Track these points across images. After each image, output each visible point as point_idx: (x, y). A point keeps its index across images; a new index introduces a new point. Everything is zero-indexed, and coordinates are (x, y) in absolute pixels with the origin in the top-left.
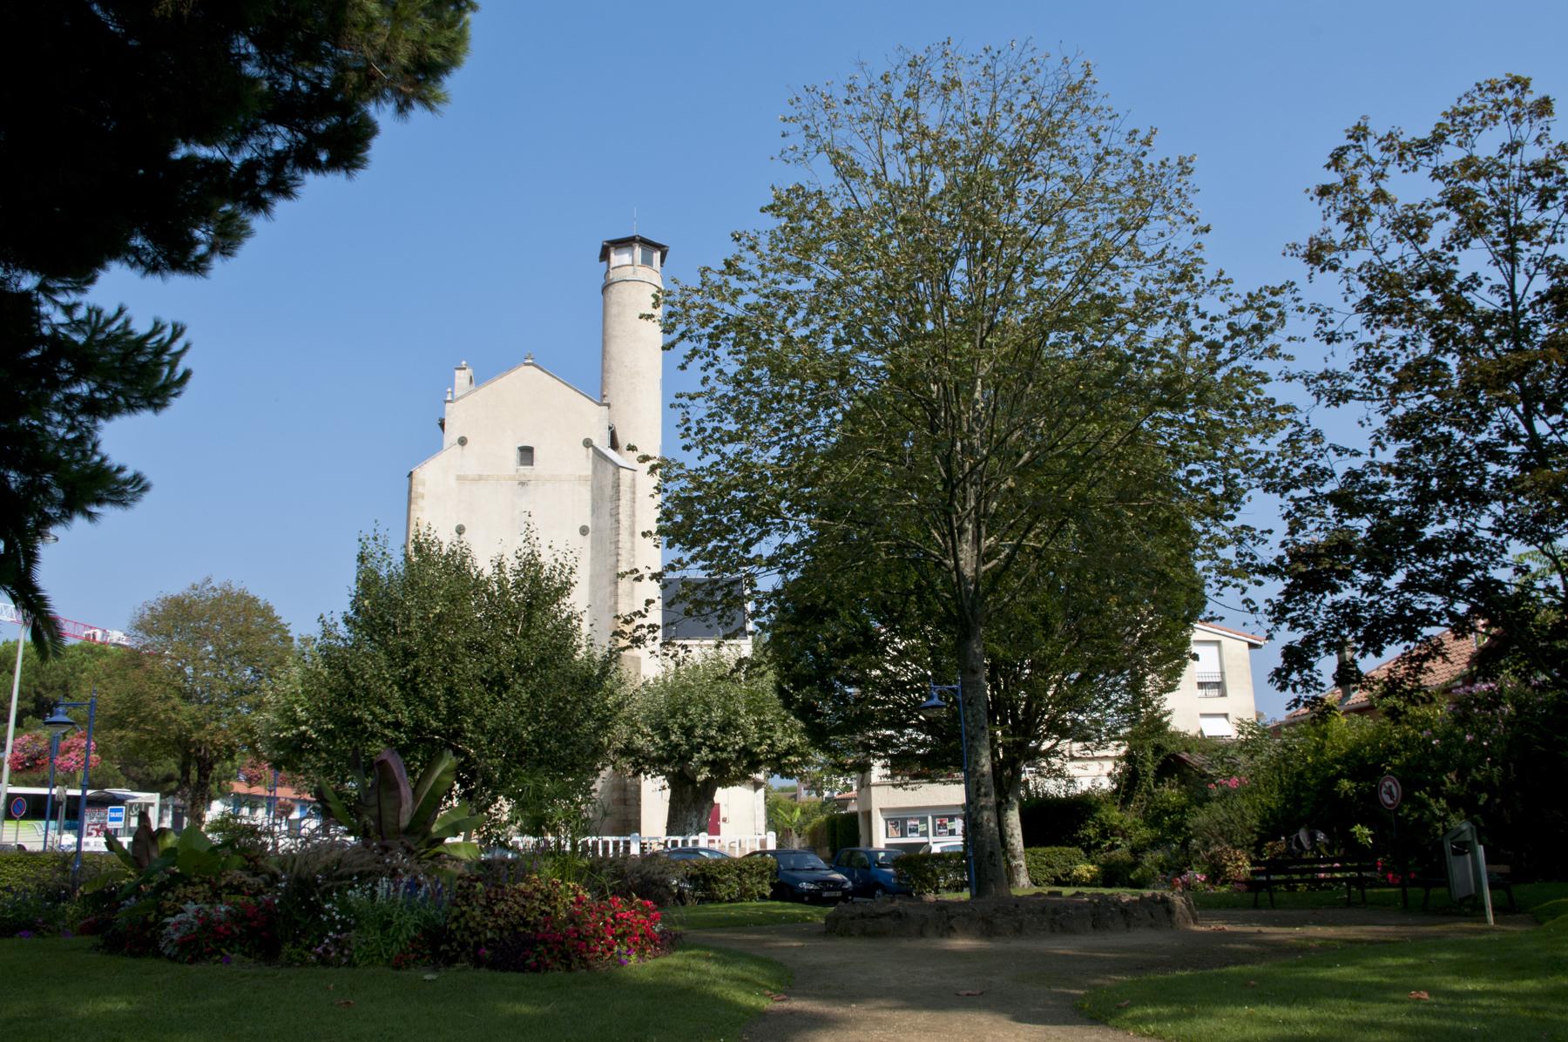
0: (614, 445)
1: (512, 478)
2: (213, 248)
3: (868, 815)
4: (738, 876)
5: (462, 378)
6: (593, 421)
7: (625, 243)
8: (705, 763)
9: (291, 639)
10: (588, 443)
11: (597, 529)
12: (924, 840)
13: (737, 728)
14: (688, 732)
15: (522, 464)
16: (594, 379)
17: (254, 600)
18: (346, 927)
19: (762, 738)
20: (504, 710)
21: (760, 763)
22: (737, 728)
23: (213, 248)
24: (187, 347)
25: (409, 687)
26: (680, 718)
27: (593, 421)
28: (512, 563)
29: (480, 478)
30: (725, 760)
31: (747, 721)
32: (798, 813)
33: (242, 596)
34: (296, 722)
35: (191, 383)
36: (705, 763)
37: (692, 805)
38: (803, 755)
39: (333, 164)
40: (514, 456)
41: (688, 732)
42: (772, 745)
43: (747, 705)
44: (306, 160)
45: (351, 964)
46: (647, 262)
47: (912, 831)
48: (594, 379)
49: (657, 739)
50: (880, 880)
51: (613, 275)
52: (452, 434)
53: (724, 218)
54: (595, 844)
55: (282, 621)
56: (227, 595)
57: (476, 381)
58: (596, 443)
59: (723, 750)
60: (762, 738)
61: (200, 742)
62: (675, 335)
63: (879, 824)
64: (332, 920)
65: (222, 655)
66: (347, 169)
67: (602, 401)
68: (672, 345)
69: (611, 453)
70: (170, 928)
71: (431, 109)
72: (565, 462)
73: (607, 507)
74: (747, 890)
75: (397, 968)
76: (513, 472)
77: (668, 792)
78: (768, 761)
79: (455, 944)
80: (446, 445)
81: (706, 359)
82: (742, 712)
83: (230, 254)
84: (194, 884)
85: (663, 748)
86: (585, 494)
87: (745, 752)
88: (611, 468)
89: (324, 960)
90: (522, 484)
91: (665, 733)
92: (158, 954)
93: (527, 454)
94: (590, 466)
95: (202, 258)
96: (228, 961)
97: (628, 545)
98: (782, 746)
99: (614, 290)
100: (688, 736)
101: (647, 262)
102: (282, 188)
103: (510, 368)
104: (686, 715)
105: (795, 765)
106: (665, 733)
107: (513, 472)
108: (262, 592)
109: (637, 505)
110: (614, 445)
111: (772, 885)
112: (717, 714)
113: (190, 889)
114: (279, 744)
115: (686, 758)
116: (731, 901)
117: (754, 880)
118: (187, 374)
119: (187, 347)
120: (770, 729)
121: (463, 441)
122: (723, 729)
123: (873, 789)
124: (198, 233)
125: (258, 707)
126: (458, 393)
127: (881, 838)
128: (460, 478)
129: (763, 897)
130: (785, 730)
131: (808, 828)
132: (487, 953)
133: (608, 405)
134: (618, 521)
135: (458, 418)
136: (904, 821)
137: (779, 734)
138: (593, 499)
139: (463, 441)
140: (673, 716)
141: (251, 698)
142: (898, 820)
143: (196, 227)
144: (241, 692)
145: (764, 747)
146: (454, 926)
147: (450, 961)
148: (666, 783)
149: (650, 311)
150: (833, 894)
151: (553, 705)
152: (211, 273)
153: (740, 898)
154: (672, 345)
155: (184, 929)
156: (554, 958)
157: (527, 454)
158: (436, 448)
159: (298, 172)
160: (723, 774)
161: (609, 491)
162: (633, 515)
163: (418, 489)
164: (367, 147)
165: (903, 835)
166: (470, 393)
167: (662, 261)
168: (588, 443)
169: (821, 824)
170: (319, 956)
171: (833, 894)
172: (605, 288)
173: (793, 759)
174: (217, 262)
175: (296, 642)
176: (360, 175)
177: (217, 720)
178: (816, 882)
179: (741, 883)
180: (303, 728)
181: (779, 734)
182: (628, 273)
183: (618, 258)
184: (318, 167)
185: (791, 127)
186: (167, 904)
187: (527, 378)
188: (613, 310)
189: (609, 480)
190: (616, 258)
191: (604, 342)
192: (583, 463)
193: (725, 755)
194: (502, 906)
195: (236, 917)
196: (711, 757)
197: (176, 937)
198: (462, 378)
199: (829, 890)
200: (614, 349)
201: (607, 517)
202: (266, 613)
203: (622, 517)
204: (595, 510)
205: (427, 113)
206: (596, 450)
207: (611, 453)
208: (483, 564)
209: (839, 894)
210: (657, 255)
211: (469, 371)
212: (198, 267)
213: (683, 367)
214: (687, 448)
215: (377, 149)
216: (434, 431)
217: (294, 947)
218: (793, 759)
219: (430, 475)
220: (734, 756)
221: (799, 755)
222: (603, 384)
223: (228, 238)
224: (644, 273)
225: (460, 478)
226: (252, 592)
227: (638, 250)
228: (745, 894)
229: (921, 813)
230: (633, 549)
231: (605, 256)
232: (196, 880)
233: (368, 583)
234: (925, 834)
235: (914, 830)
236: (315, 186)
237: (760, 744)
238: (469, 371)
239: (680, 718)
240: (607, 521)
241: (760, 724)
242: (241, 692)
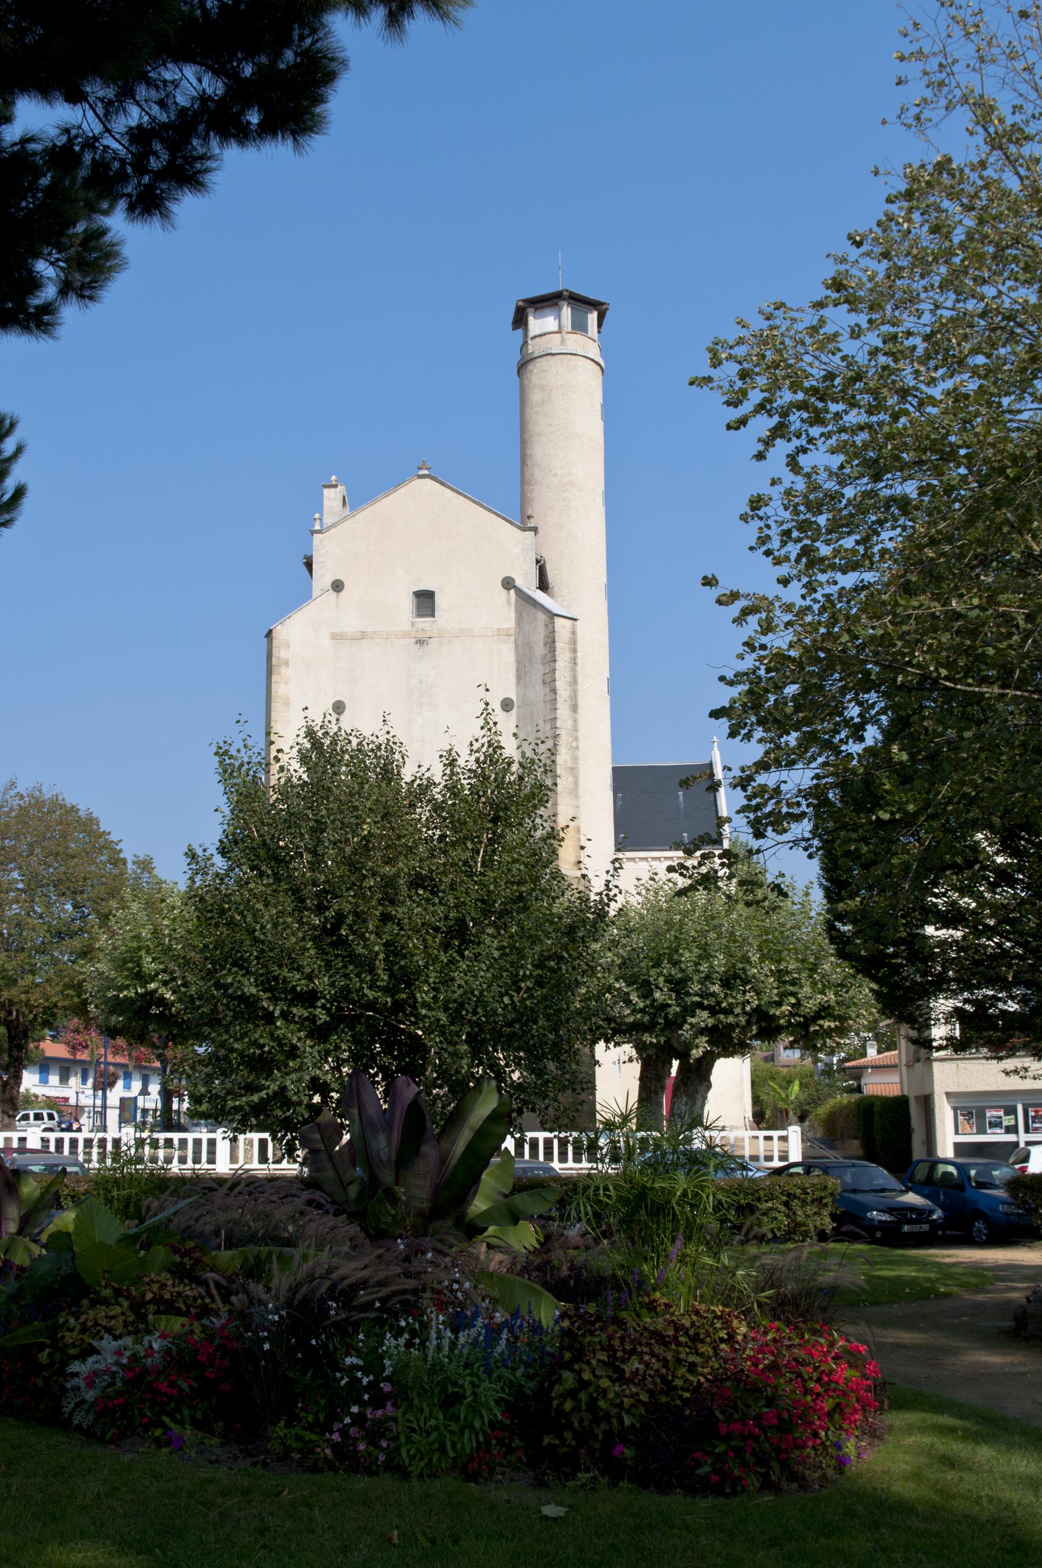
0: (543, 585)
1: (407, 635)
2: (66, 289)
3: (927, 1102)
4: (786, 1204)
5: (332, 498)
6: (512, 552)
7: (547, 302)
8: (702, 1031)
9: (124, 861)
10: (508, 584)
11: (525, 703)
12: (1011, 1138)
13: (746, 982)
14: (678, 986)
15: (420, 614)
16: (511, 492)
17: (74, 809)
18: (379, 1400)
19: (783, 995)
20: (474, 975)
21: (779, 1030)
22: (746, 982)
23: (66, 289)
24: (19, 450)
25: (330, 938)
26: (666, 968)
27: (512, 552)
28: (466, 760)
29: (363, 636)
30: (731, 1027)
31: (760, 970)
32: (796, 1087)
33: (56, 804)
34: (141, 977)
35: (27, 503)
36: (702, 1031)
37: (675, 1083)
38: (842, 1019)
39: (269, 129)
40: (408, 604)
41: (678, 986)
42: (798, 1004)
43: (760, 949)
44: (223, 120)
45: (396, 1468)
46: (580, 326)
47: (993, 1125)
48: (511, 492)
49: (634, 997)
50: (982, 1206)
51: (533, 347)
52: (322, 577)
53: (793, 225)
54: (577, 1159)
55: (113, 838)
56: (38, 803)
57: (353, 503)
58: (519, 583)
59: (728, 1012)
60: (783, 995)
61: (11, 1003)
62: (747, 407)
63: (945, 1116)
64: (355, 1382)
65: (34, 884)
66: (294, 133)
67: (524, 522)
68: (743, 422)
69: (540, 596)
70: (79, 1381)
71: (444, 16)
72: (473, 609)
73: (538, 671)
74: (798, 1225)
75: (472, 1477)
76: (407, 627)
77: (636, 1068)
78: (789, 1027)
79: (568, 1435)
80: (316, 592)
81: (796, 443)
82: (755, 958)
83: (91, 298)
84: (105, 1302)
85: (642, 1011)
86: (507, 656)
87: (760, 1015)
88: (542, 617)
89: (347, 1459)
90: (421, 642)
91: (646, 989)
92: (65, 1425)
93: (425, 601)
94: (512, 615)
95: (47, 309)
96: (178, 1445)
97: (569, 724)
98: (810, 1006)
99: (534, 368)
100: (678, 993)
101: (580, 326)
102: (188, 175)
103: (398, 482)
104: (675, 964)
105: (829, 1033)
106: (646, 989)
107: (407, 627)
108: (82, 797)
109: (579, 667)
110: (543, 585)
111: (833, 1217)
112: (719, 963)
113: (101, 1312)
114: (117, 1006)
115: (674, 1024)
116: (775, 1239)
117: (810, 1210)
118: (19, 493)
119: (19, 450)
120: (793, 983)
121: (338, 586)
122: (727, 983)
123: (936, 1066)
124: (42, 267)
125: (86, 953)
126: (328, 521)
127: (948, 1136)
128: (335, 637)
129: (822, 1237)
130: (814, 984)
131: (823, 1110)
132: (628, 1453)
133: (535, 530)
134: (554, 691)
135: (330, 554)
136: (981, 1115)
137: (807, 990)
138: (519, 662)
139: (338, 586)
140: (657, 964)
141: (77, 943)
142: (972, 1108)
143: (38, 255)
144: (60, 935)
145: (786, 1008)
146: (568, 1405)
147: (565, 1466)
148: (634, 1053)
149: (707, 371)
150: (916, 1228)
151: (540, 965)
152: (60, 331)
153: (788, 1236)
154: (743, 422)
155: (100, 1382)
156: (745, 1465)
157: (425, 601)
158: (303, 596)
159: (214, 143)
160: (726, 1042)
161: (540, 650)
162: (574, 681)
163: (280, 653)
164: (321, 100)
165: (981, 1131)
166: (345, 519)
167: (600, 324)
168: (508, 584)
169: (842, 1108)
170: (335, 1447)
171: (916, 1228)
172: (524, 365)
173: (827, 1024)
174: (70, 313)
175: (130, 865)
176: (316, 142)
177: (33, 972)
178: (889, 1210)
179: (791, 1214)
180: (153, 986)
181: (807, 990)
182: (553, 343)
183: (539, 324)
184: (242, 135)
185: (912, 69)
186: (69, 1338)
187: (422, 492)
188: (535, 397)
189: (539, 636)
190: (536, 324)
191: (524, 443)
192: (503, 611)
193: (731, 1019)
194: (635, 1364)
195: (181, 1358)
196: (711, 1022)
197: (90, 1395)
198: (332, 498)
199: (911, 1222)
200: (538, 451)
201: (539, 686)
202: (89, 825)
203: (559, 684)
204: (521, 676)
205: (437, 24)
206: (519, 592)
207: (540, 596)
208: (422, 761)
209: (926, 1227)
210: (593, 317)
211: (341, 490)
212: (39, 321)
213: (760, 456)
214: (785, 582)
215: (340, 103)
216: (301, 572)
217: (288, 1426)
218: (827, 1024)
219: (294, 634)
220: (743, 1020)
221: (835, 1018)
222: (524, 500)
223: (91, 267)
224: (575, 342)
225: (335, 637)
226: (70, 799)
227: (566, 311)
228: (794, 1232)
229: (1007, 1101)
230: (575, 729)
231: (520, 320)
232: (107, 1292)
233: (245, 791)
234: (1012, 1129)
235: (996, 1124)
236: (241, 169)
237: (779, 1004)
238: (341, 490)
239: (666, 968)
240: (538, 692)
241: (780, 975)
242: (60, 935)
